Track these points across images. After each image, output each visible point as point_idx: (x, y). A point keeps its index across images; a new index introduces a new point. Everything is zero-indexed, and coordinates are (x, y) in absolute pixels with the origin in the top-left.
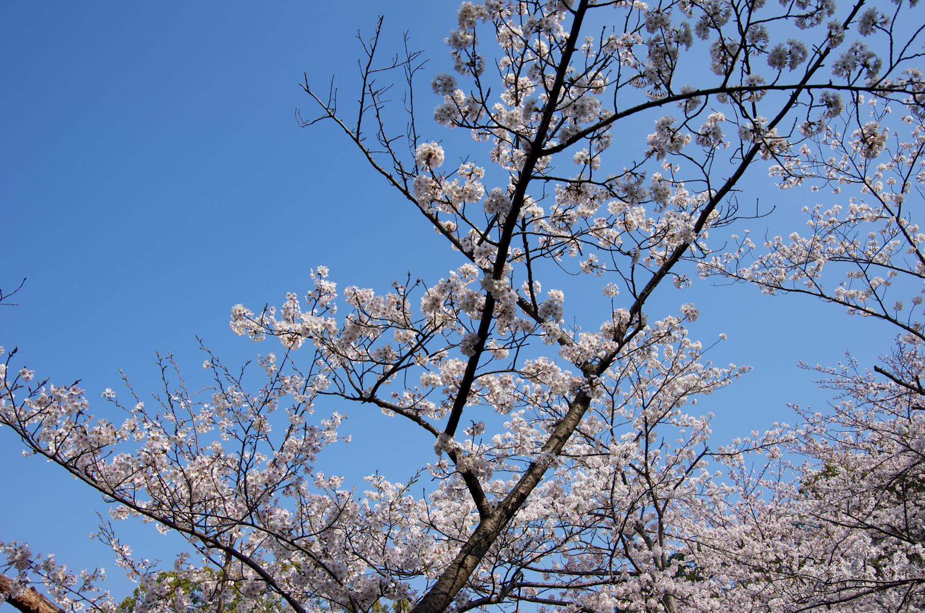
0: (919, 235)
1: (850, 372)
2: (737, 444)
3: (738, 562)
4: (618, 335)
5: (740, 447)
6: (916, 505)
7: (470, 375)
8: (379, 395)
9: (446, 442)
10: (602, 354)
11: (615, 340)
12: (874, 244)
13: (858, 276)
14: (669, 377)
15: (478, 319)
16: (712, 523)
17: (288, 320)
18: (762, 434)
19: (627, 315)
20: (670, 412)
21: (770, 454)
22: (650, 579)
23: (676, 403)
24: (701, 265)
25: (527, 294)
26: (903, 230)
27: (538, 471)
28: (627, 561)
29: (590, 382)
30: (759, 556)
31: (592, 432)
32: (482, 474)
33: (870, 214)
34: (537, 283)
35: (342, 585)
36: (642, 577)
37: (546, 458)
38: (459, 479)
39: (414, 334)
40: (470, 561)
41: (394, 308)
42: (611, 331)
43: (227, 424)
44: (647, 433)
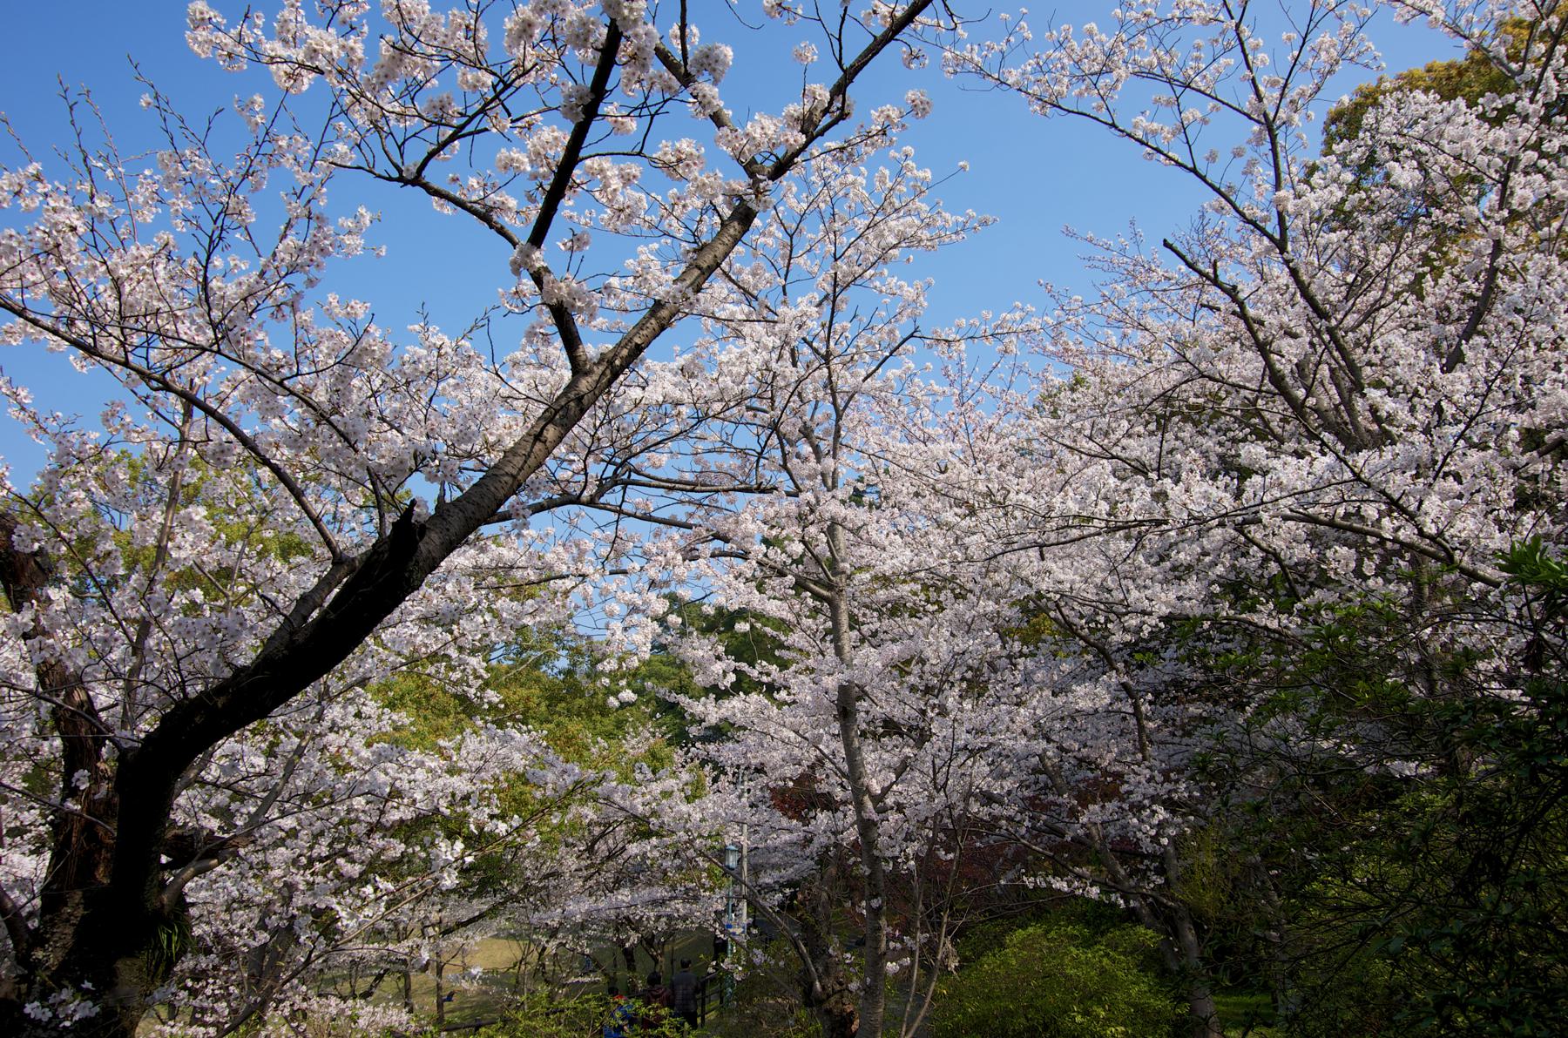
0: (1260, 56)
1: (1131, 250)
2: (959, 327)
3: (936, 492)
4: (810, 127)
5: (962, 332)
6: (1177, 438)
7: (572, 156)
8: (429, 175)
9: (528, 256)
10: (780, 153)
11: (802, 131)
12: (1197, 59)
13: (1168, 103)
14: (877, 218)
15: (592, 64)
16: (910, 438)
17: (285, 42)
18: (996, 317)
19: (824, 95)
20: (871, 271)
21: (1001, 347)
22: (813, 501)
23: (882, 258)
24: (948, 55)
25: (676, 45)
26: (1242, 44)
27: (664, 313)
28: (784, 476)
29: (758, 193)
30: (965, 485)
31: (755, 287)
32: (580, 310)
33: (1203, 13)
34: (693, 29)
35: (356, 451)
36: (802, 496)
37: (679, 295)
38: (547, 317)
39: (490, 80)
40: (551, 433)
41: (461, 34)
42: (797, 119)
43: (182, 204)
44: (835, 298)
